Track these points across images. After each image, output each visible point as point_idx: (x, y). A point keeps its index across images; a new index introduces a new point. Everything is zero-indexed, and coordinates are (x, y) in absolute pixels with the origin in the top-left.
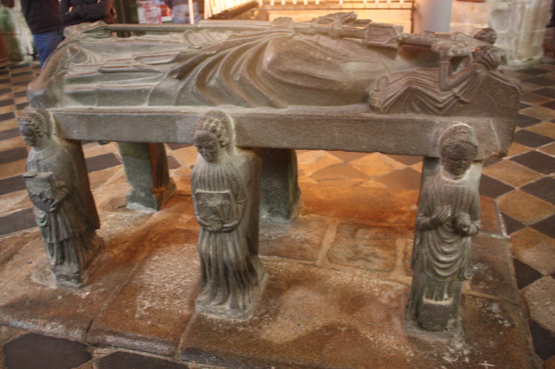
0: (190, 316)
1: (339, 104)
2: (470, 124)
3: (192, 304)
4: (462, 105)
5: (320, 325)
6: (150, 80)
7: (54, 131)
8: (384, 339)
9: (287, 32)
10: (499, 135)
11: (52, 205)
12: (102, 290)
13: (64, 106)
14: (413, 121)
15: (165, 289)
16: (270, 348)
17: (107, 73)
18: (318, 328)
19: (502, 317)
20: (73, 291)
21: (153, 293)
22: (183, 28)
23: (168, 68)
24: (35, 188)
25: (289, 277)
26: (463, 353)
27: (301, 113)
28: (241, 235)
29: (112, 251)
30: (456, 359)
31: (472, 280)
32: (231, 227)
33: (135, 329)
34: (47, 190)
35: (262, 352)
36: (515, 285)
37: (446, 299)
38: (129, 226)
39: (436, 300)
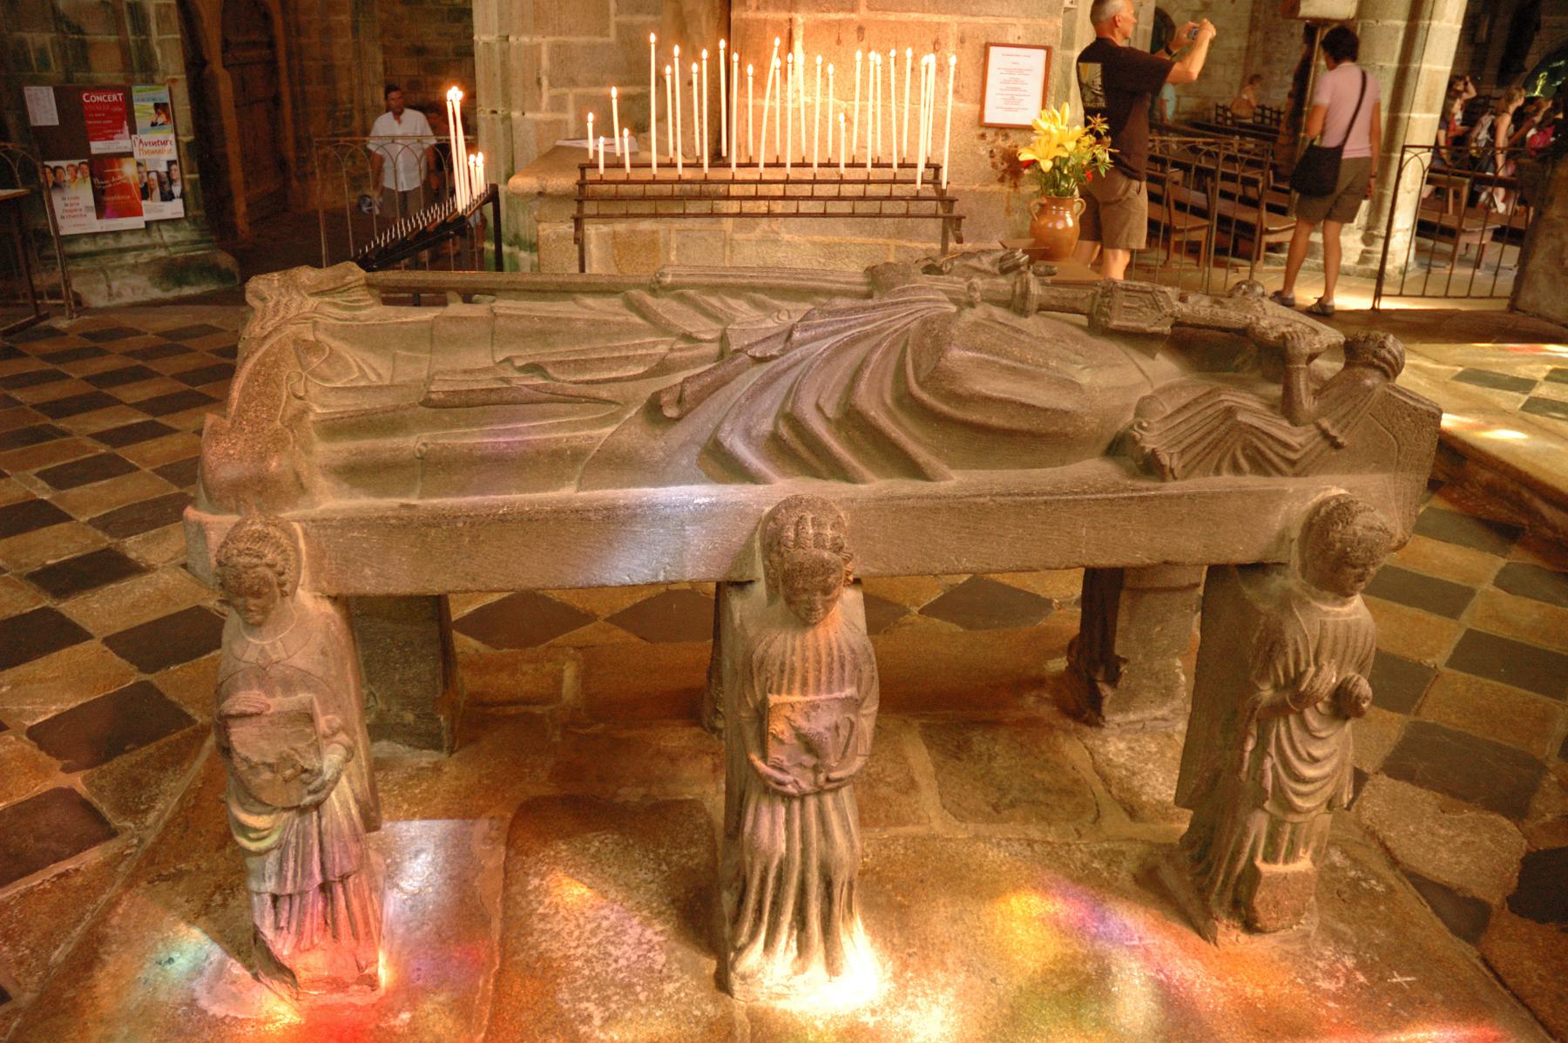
6: (582, 422)
8: (1185, 970)
13: (319, 504)
21: (590, 978)
24: (263, 744)
39: (1286, 862)
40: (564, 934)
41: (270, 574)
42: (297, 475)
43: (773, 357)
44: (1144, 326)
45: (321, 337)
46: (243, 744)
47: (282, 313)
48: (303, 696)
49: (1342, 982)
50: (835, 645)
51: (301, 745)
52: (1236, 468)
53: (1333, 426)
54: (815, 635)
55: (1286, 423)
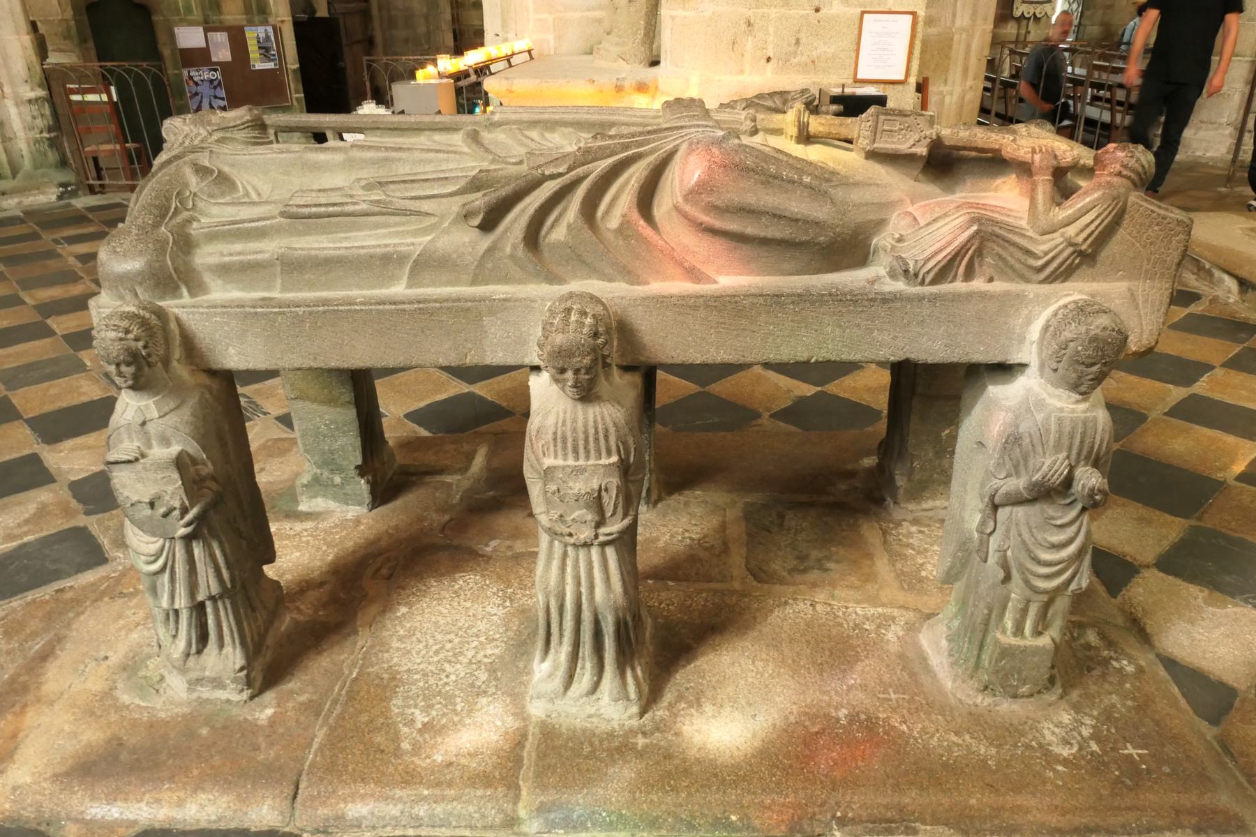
1: (819, 271)
6: (408, 232)
7: (177, 353)
11: (182, 522)
16: (716, 775)
17: (299, 218)
18: (792, 719)
20: (235, 711)
21: (423, 689)
23: (455, 205)
24: (139, 486)
34: (170, 489)
35: (702, 786)
38: (319, 549)
43: (560, 175)
49: (1075, 748)
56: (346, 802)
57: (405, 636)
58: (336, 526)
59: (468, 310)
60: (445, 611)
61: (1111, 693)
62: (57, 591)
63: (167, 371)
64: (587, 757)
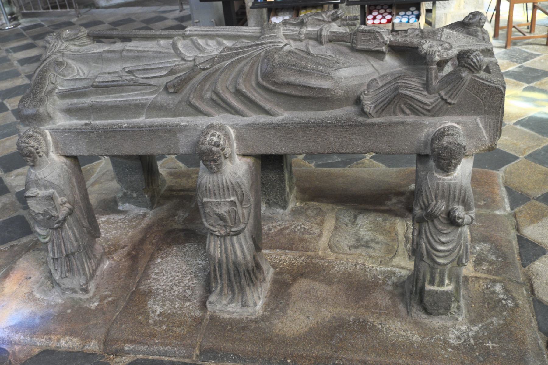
0: (202, 319)
2: (458, 123)
3: (203, 305)
4: (449, 106)
5: (329, 316)
7: (52, 148)
9: (279, 42)
10: (487, 132)
12: (110, 299)
14: (403, 123)
15: (174, 292)
16: (284, 342)
19: (505, 297)
21: (162, 297)
22: (171, 35)
24: (38, 206)
25: (293, 270)
26: (468, 335)
27: (298, 120)
28: (248, 237)
29: (113, 258)
30: (462, 341)
31: (475, 262)
32: (239, 231)
33: (152, 335)
36: (518, 263)
37: (448, 285)
40: (161, 281)
41: (33, 149)
42: (48, 114)
43: (207, 69)
44: (372, 48)
45: (65, 59)
46: (32, 206)
47: (53, 50)
48: (51, 191)
50: (224, 181)
51: (50, 208)
52: (404, 113)
53: (446, 95)
54: (217, 177)
55: (426, 93)
56: (125, 344)
57: (158, 273)
58: (134, 218)
59: (170, 130)
60: (178, 262)
61: (494, 316)
62: (11, 246)
63: (48, 157)
64: (228, 331)
